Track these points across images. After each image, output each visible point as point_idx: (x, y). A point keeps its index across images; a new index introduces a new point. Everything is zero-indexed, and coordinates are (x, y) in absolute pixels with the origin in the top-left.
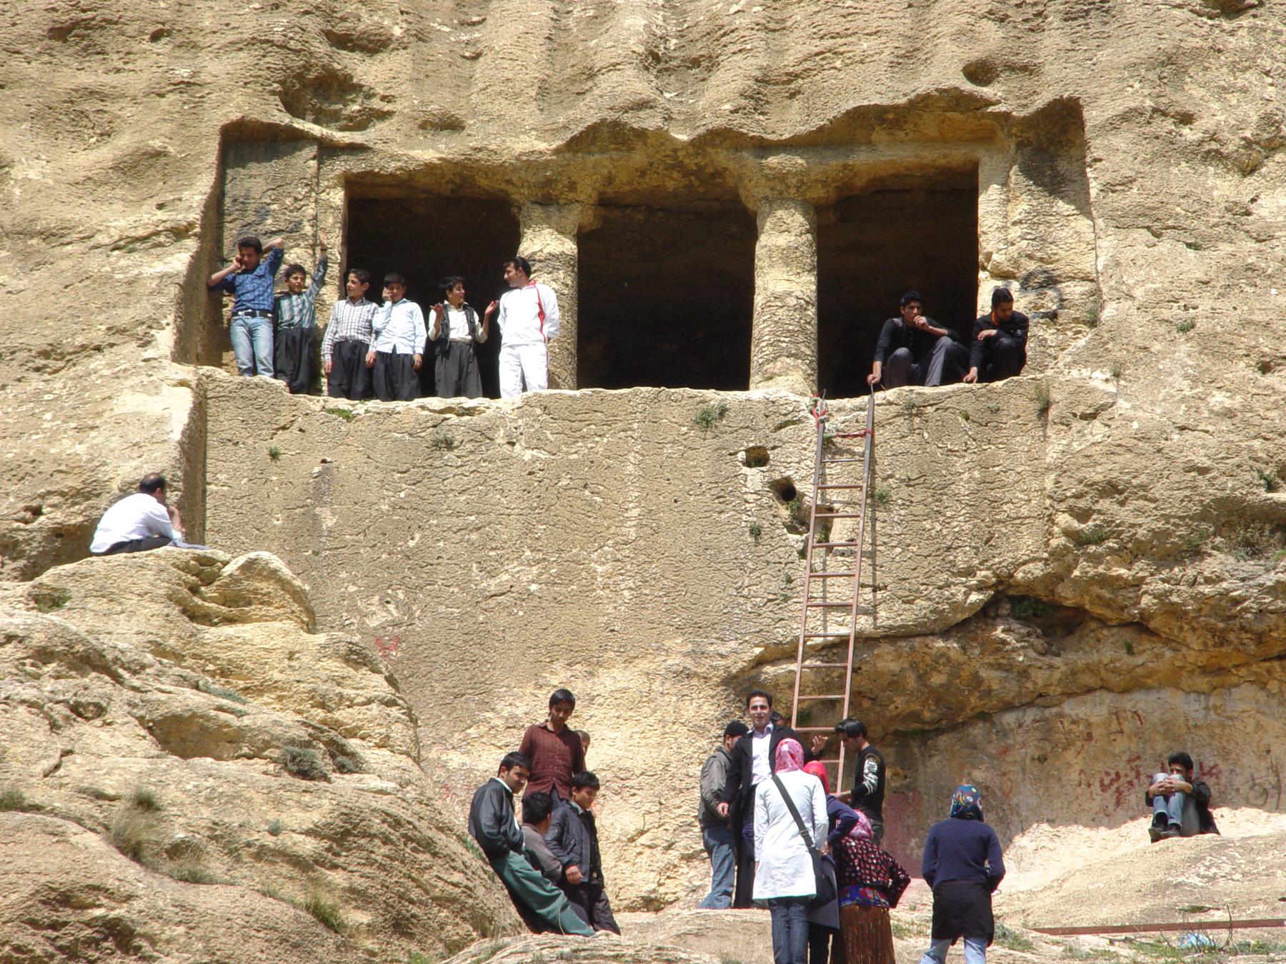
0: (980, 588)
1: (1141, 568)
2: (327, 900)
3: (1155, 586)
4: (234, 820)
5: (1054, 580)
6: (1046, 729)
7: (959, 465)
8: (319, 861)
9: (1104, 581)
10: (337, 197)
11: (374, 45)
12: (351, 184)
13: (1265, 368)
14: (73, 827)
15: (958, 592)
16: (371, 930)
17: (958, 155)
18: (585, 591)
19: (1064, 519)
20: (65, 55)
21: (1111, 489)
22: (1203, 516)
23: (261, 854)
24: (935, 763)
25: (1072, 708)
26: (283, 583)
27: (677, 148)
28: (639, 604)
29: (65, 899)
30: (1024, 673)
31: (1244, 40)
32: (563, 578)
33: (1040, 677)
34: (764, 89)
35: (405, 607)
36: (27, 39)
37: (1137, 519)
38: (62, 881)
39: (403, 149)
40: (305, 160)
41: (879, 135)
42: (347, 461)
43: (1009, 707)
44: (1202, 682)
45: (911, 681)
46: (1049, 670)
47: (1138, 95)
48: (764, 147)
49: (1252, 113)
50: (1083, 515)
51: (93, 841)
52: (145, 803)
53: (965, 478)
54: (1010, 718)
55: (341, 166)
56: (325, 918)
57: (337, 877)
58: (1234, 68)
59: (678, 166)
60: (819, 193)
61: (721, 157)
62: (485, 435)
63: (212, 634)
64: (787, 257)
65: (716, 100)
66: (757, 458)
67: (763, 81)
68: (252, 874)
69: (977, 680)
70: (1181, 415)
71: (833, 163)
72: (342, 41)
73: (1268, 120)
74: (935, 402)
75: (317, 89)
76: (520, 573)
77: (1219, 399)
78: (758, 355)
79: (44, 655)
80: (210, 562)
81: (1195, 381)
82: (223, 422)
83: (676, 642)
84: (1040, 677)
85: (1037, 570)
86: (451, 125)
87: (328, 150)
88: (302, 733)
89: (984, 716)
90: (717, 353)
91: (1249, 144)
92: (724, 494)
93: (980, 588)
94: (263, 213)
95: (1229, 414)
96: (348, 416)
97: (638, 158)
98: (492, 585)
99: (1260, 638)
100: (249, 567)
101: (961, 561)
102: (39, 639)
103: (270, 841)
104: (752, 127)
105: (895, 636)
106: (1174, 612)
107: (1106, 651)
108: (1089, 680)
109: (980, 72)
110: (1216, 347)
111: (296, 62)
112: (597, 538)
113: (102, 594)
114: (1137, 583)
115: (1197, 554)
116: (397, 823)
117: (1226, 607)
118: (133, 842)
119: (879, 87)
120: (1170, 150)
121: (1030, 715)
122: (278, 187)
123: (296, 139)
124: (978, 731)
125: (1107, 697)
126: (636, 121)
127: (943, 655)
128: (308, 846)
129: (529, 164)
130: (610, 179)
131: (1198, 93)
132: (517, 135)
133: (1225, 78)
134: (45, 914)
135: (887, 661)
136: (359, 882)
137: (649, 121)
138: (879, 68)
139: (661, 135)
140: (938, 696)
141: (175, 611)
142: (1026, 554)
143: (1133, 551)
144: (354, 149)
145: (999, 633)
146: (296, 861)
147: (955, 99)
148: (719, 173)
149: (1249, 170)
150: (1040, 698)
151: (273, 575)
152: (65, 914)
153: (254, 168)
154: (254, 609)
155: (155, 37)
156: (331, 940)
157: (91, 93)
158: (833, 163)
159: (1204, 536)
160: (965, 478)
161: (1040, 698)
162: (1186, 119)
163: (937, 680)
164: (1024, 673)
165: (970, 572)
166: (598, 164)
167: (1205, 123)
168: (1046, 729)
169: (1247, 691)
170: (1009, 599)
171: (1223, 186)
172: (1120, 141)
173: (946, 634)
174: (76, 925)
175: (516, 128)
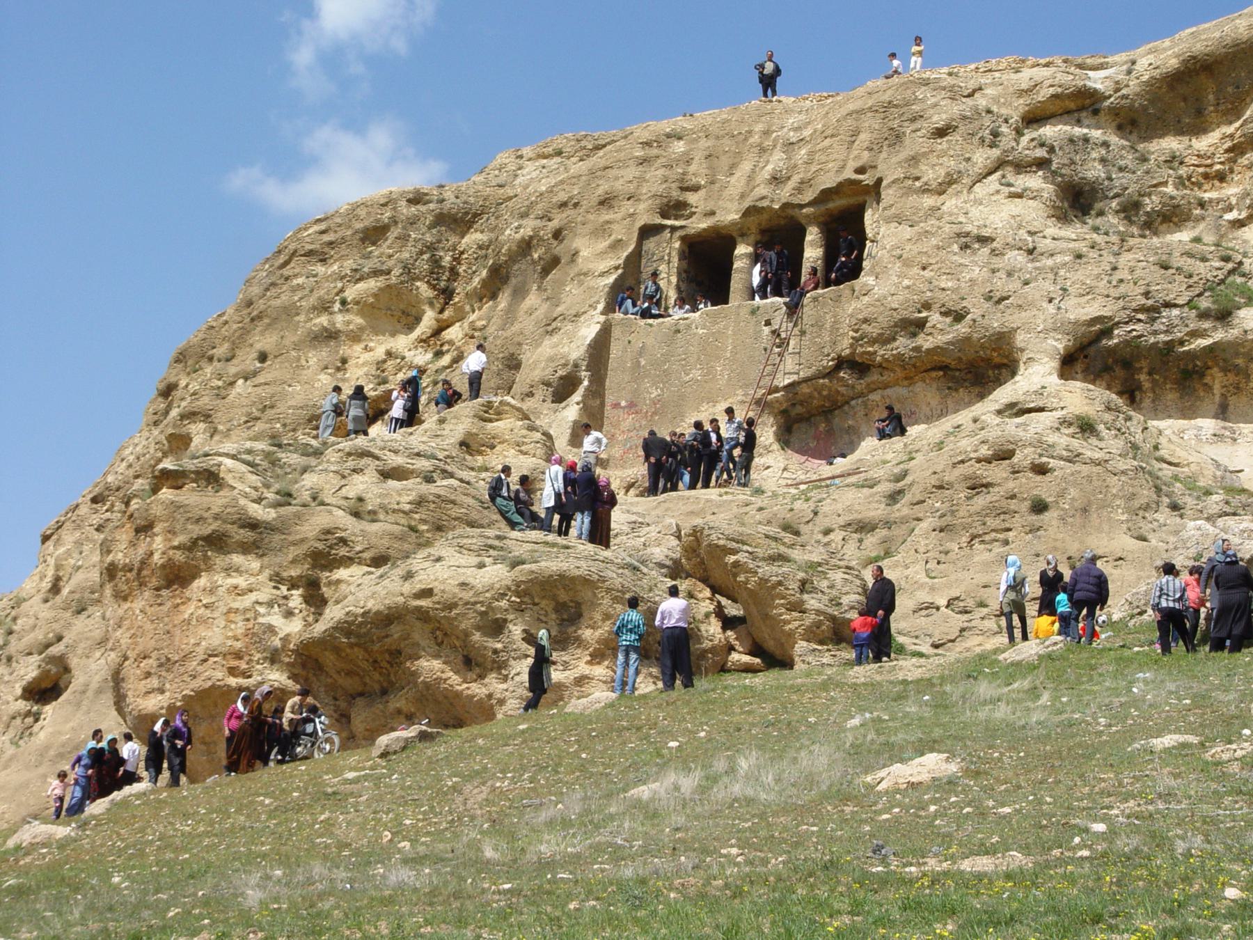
0: (833, 360)
1: (876, 347)
2: (413, 523)
3: (882, 352)
4: (386, 502)
5: (853, 353)
6: (865, 404)
7: (828, 317)
8: (411, 511)
9: (865, 353)
10: (677, 245)
11: (695, 189)
12: (683, 239)
13: (924, 269)
14: (335, 509)
15: (825, 363)
16: (428, 531)
17: (861, 199)
18: (715, 376)
19: (851, 333)
20: (603, 210)
21: (865, 321)
22: (896, 325)
23: (394, 511)
24: (837, 420)
25: (871, 397)
26: (513, 407)
27: (776, 211)
28: (730, 379)
29: (328, 532)
30: (853, 387)
31: (945, 146)
32: (708, 374)
33: (859, 387)
34: (799, 190)
35: (662, 390)
36: (592, 207)
37: (872, 330)
38: (327, 526)
39: (698, 224)
40: (667, 234)
41: (834, 197)
42: (650, 341)
43: (853, 399)
44: (906, 383)
45: (816, 394)
46: (861, 385)
47: (899, 173)
48: (802, 206)
49: (942, 172)
50: (856, 331)
51: (341, 513)
52: (360, 499)
53: (829, 320)
54: (853, 403)
55: (678, 234)
56: (413, 529)
57: (417, 516)
58: (938, 157)
59: (779, 216)
60: (822, 219)
61: (790, 212)
62: (689, 326)
63: (490, 425)
64: (812, 243)
65: (785, 194)
66: (768, 323)
67: (802, 183)
68: (391, 518)
69: (838, 392)
70: (893, 291)
71: (823, 208)
72: (684, 189)
73: (948, 174)
74: (822, 295)
75: (674, 208)
76: (696, 374)
77: (906, 282)
78: (731, 295)
79: (349, 454)
80: (489, 402)
81: (899, 277)
82: (616, 332)
83: (740, 392)
84: (859, 387)
85: (848, 351)
86: (713, 213)
87: (673, 229)
88: (431, 469)
89: (847, 403)
90: (719, 294)
91: (940, 184)
92: (757, 336)
93: (833, 360)
94: (653, 254)
95: (908, 287)
96: (651, 325)
97: (765, 216)
98: (687, 378)
99: (914, 366)
100: (501, 402)
101: (826, 351)
102: (347, 450)
103: (396, 507)
104: (796, 201)
105: (806, 380)
106: (887, 360)
107: (874, 377)
108: (872, 386)
109: (861, 170)
110: (907, 263)
111: (665, 200)
112: (718, 358)
113: (455, 417)
114: (875, 352)
115: (894, 339)
116: (439, 496)
117: (900, 357)
118: (1147, 403)
119: (829, 181)
120: (910, 191)
121: (860, 400)
122: (658, 244)
123: (663, 227)
124: (846, 408)
125: (880, 391)
126: (760, 204)
127: (823, 384)
128: (407, 507)
129: (733, 223)
130: (760, 224)
131: (924, 168)
132: (730, 215)
133: (935, 160)
134: (323, 537)
135: (805, 389)
136: (424, 517)
137: (765, 203)
138: (832, 174)
139: (769, 208)
140: (828, 398)
141: (476, 420)
142: (844, 347)
143: (873, 342)
144: (682, 227)
145: (842, 374)
146: (404, 512)
147: (850, 182)
148: (792, 217)
149: (941, 193)
150: (861, 395)
151: (508, 404)
152: (329, 536)
153: (652, 239)
154: (504, 416)
155: (629, 199)
156: (414, 535)
157: (608, 222)
158: (823, 208)
159: (896, 333)
160: (829, 320)
161: (861, 395)
162: (918, 179)
163: (825, 393)
164: (853, 387)
165: (828, 355)
166: (753, 220)
167: (924, 179)
168: (865, 404)
169: (920, 384)
170: (841, 363)
171: (929, 201)
172: (890, 192)
173: (823, 378)
174: (332, 539)
175: (729, 212)
